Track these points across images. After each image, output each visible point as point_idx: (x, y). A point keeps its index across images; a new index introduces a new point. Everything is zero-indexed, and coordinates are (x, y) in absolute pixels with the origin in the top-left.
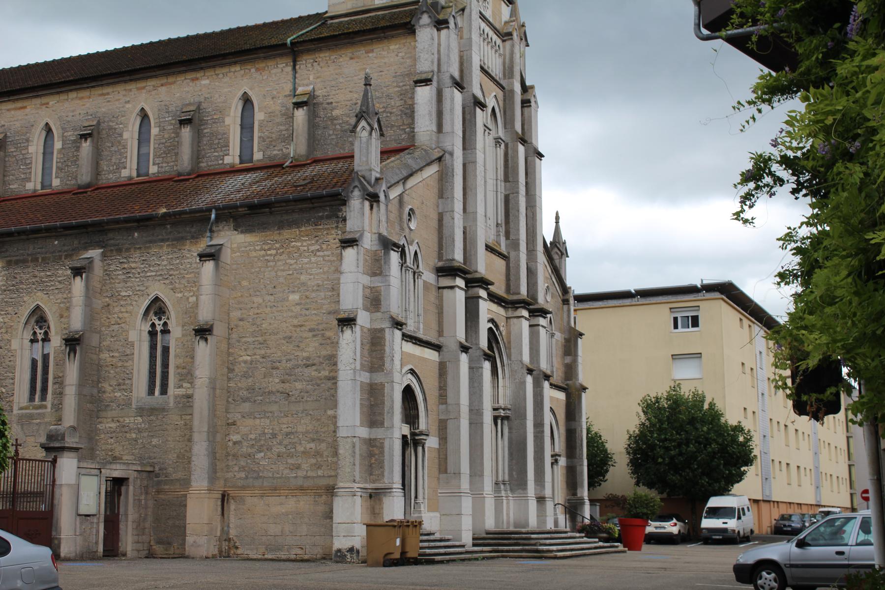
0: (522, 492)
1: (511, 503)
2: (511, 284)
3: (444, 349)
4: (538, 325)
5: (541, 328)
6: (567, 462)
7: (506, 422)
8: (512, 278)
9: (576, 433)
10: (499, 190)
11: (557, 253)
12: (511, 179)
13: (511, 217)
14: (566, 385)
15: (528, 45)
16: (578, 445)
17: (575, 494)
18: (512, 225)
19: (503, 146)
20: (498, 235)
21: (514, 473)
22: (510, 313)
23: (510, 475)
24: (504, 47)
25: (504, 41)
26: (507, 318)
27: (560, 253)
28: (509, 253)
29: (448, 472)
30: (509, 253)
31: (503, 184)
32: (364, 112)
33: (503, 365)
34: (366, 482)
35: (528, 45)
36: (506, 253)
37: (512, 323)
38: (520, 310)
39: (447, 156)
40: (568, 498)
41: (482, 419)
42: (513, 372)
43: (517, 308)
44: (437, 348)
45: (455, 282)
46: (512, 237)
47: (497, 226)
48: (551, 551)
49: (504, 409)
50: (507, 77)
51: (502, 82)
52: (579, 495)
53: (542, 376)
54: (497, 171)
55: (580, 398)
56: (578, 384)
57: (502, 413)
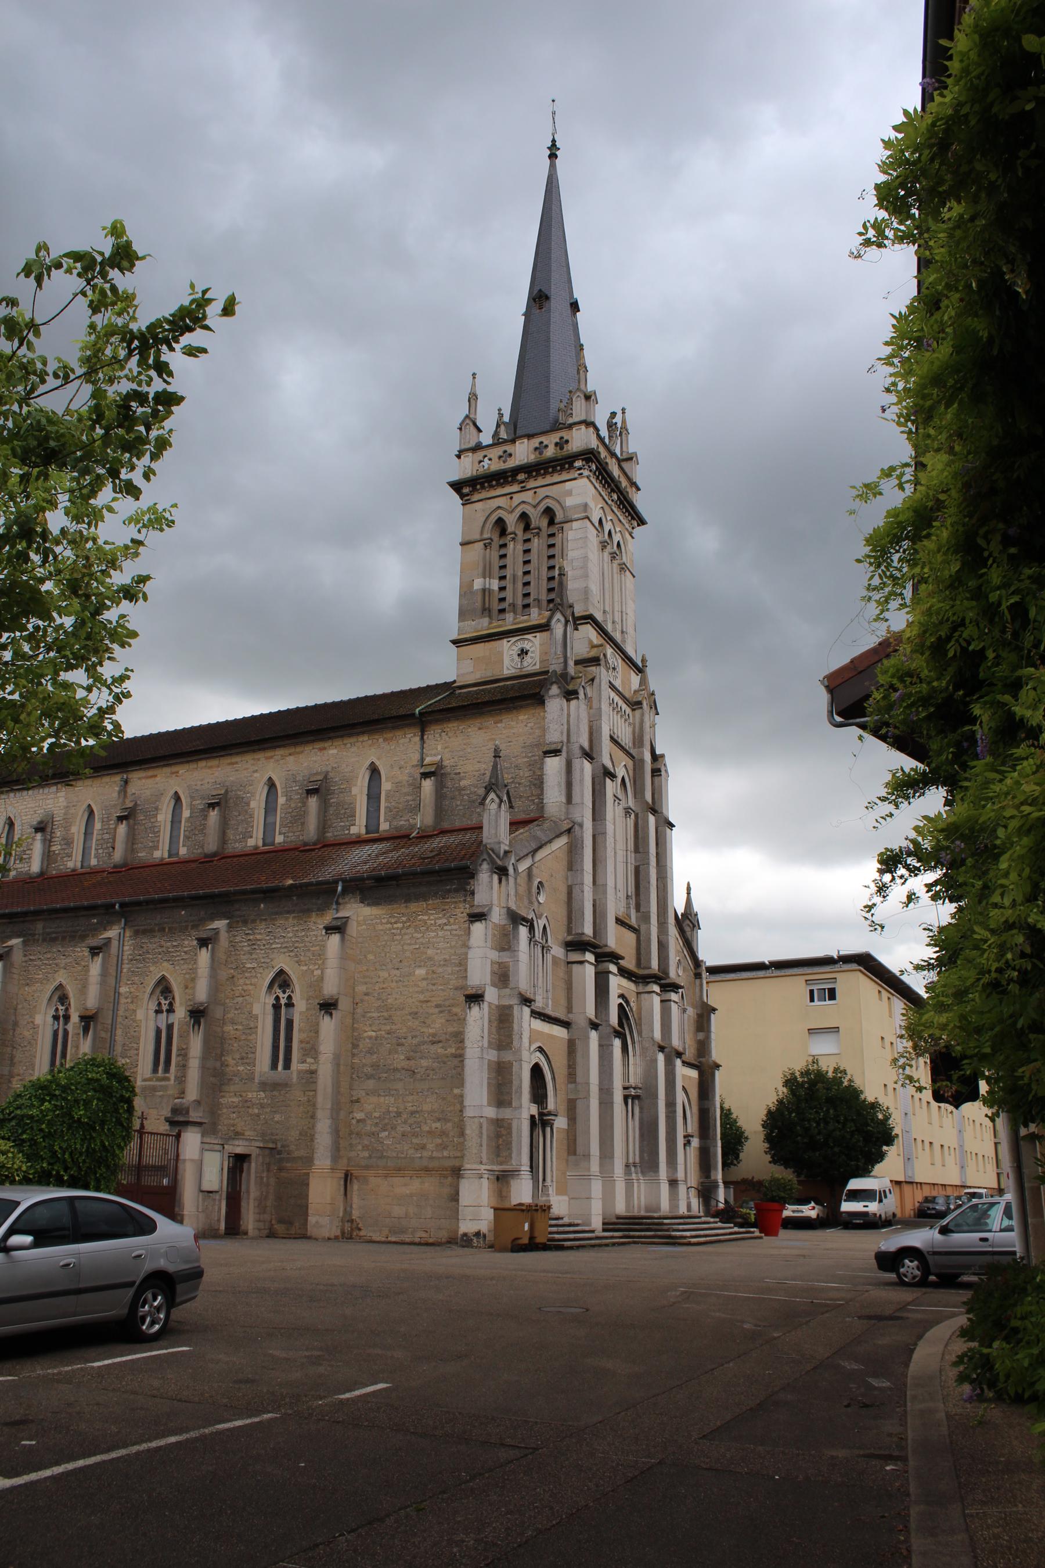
1: (642, 1186)
3: (573, 1026)
4: (670, 1000)
6: (700, 1143)
7: (637, 1102)
9: (709, 1112)
10: (629, 861)
12: (641, 850)
13: (642, 889)
15: (658, 714)
17: (708, 1176)
18: (642, 897)
19: (633, 816)
20: (628, 908)
21: (645, 1155)
22: (641, 988)
23: (641, 1157)
25: (633, 710)
26: (638, 993)
28: (639, 926)
30: (639, 926)
33: (633, 1042)
34: (493, 1164)
35: (658, 714)
38: (651, 985)
41: (613, 1099)
42: (644, 1050)
43: (648, 983)
44: (566, 1024)
46: (642, 909)
48: (685, 1237)
51: (631, 751)
53: (673, 1053)
55: (713, 1075)
57: (633, 1092)
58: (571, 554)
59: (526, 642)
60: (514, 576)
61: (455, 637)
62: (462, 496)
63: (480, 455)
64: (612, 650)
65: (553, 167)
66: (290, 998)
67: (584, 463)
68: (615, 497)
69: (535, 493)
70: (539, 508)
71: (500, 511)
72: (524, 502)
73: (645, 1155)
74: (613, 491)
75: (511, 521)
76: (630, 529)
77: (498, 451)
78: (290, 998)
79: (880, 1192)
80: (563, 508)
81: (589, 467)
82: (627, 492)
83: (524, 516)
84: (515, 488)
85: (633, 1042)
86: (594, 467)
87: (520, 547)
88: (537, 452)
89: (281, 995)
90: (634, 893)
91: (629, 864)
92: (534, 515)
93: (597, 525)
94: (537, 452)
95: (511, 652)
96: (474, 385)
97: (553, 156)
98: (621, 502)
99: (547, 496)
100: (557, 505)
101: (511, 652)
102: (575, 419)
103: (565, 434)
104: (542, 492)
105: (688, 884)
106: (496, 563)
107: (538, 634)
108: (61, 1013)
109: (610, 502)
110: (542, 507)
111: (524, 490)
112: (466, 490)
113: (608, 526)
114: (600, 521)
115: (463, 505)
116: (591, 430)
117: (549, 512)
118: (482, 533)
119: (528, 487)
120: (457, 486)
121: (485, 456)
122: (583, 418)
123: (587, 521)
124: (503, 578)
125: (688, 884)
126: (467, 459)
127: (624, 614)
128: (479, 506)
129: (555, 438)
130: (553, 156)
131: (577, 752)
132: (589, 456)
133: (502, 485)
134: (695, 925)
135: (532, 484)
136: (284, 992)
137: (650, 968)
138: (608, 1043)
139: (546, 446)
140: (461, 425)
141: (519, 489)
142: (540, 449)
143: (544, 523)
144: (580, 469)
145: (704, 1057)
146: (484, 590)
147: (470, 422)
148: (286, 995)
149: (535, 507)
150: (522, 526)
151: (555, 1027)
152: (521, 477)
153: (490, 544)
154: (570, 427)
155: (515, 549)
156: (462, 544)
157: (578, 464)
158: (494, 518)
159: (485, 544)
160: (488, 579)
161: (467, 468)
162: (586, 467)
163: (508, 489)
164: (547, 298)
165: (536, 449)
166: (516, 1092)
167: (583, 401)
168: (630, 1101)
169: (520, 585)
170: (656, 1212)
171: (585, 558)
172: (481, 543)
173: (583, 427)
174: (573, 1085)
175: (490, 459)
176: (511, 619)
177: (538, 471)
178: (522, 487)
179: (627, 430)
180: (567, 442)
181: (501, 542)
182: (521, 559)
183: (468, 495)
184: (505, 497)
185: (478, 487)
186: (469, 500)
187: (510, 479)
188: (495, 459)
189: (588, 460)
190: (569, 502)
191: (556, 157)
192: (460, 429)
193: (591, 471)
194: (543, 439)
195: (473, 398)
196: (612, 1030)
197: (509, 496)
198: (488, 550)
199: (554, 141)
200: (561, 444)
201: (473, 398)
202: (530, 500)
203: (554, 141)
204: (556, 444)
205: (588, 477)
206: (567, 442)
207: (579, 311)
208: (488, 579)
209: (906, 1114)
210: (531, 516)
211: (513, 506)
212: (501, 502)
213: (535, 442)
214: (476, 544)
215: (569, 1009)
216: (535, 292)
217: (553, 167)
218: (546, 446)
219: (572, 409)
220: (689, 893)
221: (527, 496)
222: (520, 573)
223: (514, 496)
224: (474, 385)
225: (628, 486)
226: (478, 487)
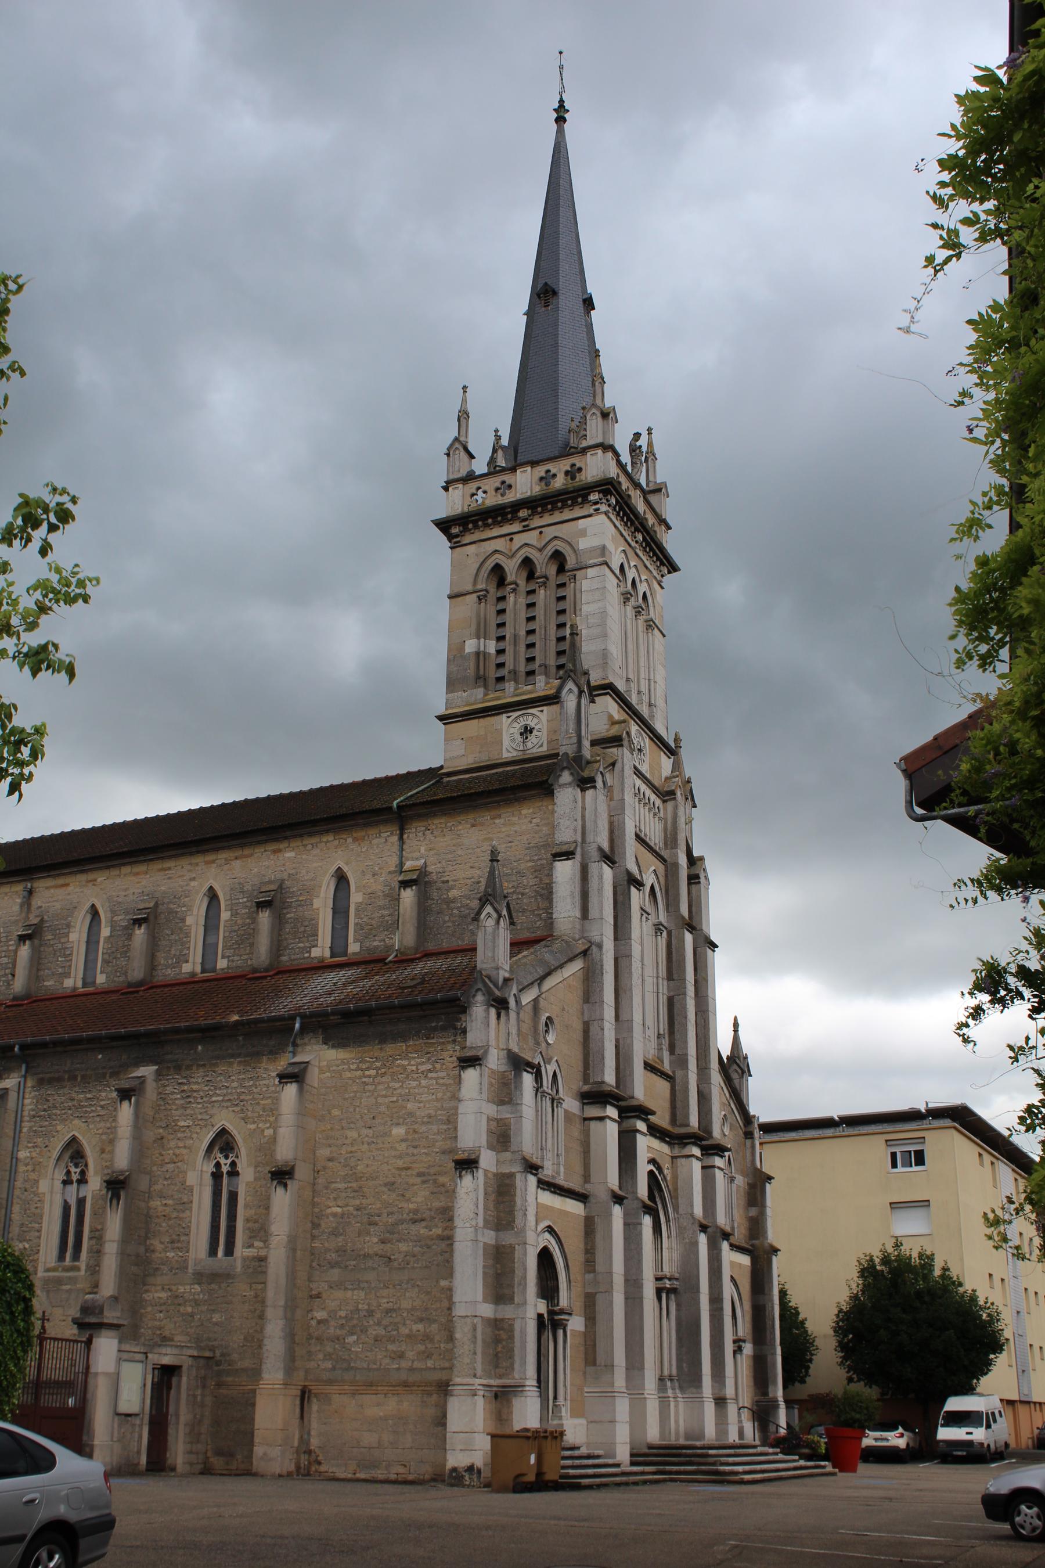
0: (694, 1390)
2: (678, 1113)
3: (592, 1200)
4: (714, 1167)
5: (717, 1170)
6: (754, 1350)
7: (673, 1296)
8: (679, 1104)
9: (765, 1310)
10: (661, 991)
11: (737, 1071)
13: (677, 1027)
14: (752, 1245)
15: (695, 807)
16: (768, 1326)
17: (765, 1393)
18: (677, 1036)
19: (665, 934)
20: (660, 1049)
21: (685, 1365)
23: (679, 1367)
24: (665, 809)
25: (664, 802)
26: (673, 1158)
27: (740, 1071)
28: (674, 1072)
29: (598, 1363)
30: (674, 1072)
31: (665, 982)
32: (490, 895)
34: (490, 1377)
35: (695, 807)
36: (670, 1073)
37: (679, 1164)
38: (689, 1147)
39: (594, 949)
40: (756, 1398)
42: (681, 1230)
43: (686, 1144)
44: (582, 1197)
45: (605, 1112)
46: (678, 1051)
47: (658, 1038)
49: (670, 1279)
50: (669, 847)
51: (662, 853)
52: (771, 1395)
53: (719, 1234)
54: (657, 967)
56: (766, 1245)
57: (668, 1284)
58: (586, 609)
59: (530, 718)
60: (515, 637)
61: (442, 710)
62: (450, 537)
63: (472, 486)
64: (637, 727)
65: (560, 133)
66: (233, 1164)
67: (601, 495)
68: (640, 537)
69: (541, 533)
70: (545, 553)
71: (497, 556)
72: (526, 544)
73: (685, 1365)
74: (637, 530)
75: (511, 567)
76: (659, 577)
77: (495, 482)
78: (233, 1164)
79: (987, 1414)
80: (575, 551)
81: (608, 500)
82: (655, 532)
83: (527, 562)
84: (516, 527)
85: (668, 1220)
86: (613, 501)
87: (523, 601)
88: (543, 483)
89: (223, 1161)
90: (666, 1031)
91: (661, 995)
92: (540, 560)
93: (617, 572)
94: (543, 483)
95: (512, 731)
96: (464, 401)
97: (560, 120)
98: (648, 545)
99: (555, 537)
100: (568, 548)
101: (512, 731)
102: (590, 441)
103: (577, 461)
104: (550, 532)
105: (736, 1019)
106: (493, 620)
107: (545, 708)
108: (225, 1169)
109: (633, 544)
110: (549, 551)
111: (526, 529)
112: (455, 530)
113: (631, 574)
114: (622, 567)
115: (451, 548)
116: (610, 454)
117: (558, 556)
118: (475, 583)
119: (532, 526)
120: (444, 525)
121: (479, 488)
122: (599, 440)
123: (605, 567)
124: (501, 638)
125: (736, 1019)
126: (456, 491)
127: (652, 682)
128: (471, 549)
129: (565, 465)
130: (560, 120)
131: (595, 855)
132: (607, 487)
133: (500, 524)
134: (745, 1071)
135: (537, 522)
136: (226, 1157)
137: (688, 1125)
138: (635, 1221)
139: (554, 476)
140: (448, 449)
141: (521, 529)
142: (546, 479)
143: (552, 570)
144: (596, 503)
145: (757, 1238)
146: (478, 654)
147: (460, 446)
148: (229, 1161)
149: (540, 550)
150: (524, 574)
151: (568, 1200)
152: (523, 513)
153: (485, 596)
154: (584, 451)
155: (516, 603)
156: (450, 597)
157: (594, 497)
158: (490, 564)
159: (478, 597)
160: (482, 640)
161: (455, 503)
162: (604, 501)
163: (507, 529)
164: (555, 293)
165: (541, 479)
166: (520, 1284)
167: (600, 419)
168: (664, 1296)
169: (522, 648)
170: (698, 1439)
171: (604, 614)
172: (475, 596)
173: (600, 452)
174: (592, 1275)
175: (485, 492)
176: (512, 689)
177: (544, 506)
178: (524, 527)
179: (654, 455)
180: (580, 470)
181: (499, 594)
182: (523, 615)
183: (457, 536)
184: (503, 539)
185: (470, 526)
186: (459, 542)
187: (509, 516)
188: (491, 492)
189: (606, 493)
190: (583, 544)
191: (565, 120)
192: (448, 455)
193: (609, 505)
194: (550, 466)
195: (463, 416)
196: (641, 1205)
197: (508, 538)
198: (483, 604)
199: (561, 101)
200: (573, 473)
201: (463, 416)
202: (534, 542)
203: (561, 101)
204: (567, 473)
205: (606, 513)
206: (580, 470)
207: (593, 308)
208: (482, 640)
209: (1018, 1312)
210: (536, 562)
211: (514, 549)
212: (499, 544)
213: (541, 471)
214: (468, 597)
215: (587, 1178)
216: (540, 286)
217: (560, 133)
218: (554, 476)
219: (585, 430)
220: (736, 1031)
221: (531, 537)
222: (523, 633)
223: (515, 537)
224: (464, 401)
225: (656, 524)
226: (470, 526)
